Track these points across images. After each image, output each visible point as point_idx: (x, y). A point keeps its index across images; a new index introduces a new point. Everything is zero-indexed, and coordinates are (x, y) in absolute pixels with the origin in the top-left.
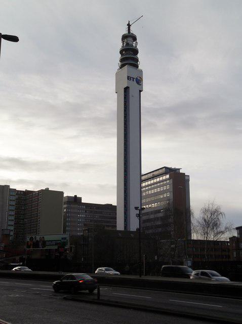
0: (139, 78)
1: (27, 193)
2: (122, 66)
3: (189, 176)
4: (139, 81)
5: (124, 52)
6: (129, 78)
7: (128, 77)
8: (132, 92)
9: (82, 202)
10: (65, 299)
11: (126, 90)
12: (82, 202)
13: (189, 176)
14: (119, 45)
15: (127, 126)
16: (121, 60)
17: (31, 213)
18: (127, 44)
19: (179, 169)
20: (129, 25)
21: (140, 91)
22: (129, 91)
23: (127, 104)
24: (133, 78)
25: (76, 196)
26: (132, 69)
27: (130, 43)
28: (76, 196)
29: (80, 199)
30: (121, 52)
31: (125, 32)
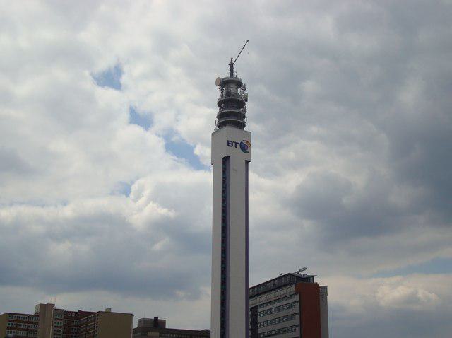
0: (245, 143)
1: (81, 314)
2: (221, 125)
3: (326, 288)
4: (245, 147)
5: (223, 105)
6: (229, 143)
7: (228, 141)
8: (235, 164)
9: (167, 327)
10: (175, 160)
11: (226, 160)
12: (167, 327)
13: (326, 288)
14: (217, 94)
15: (226, 245)
16: (220, 116)
17: (88, 323)
18: (228, 94)
19: (313, 277)
20: (232, 65)
21: (247, 162)
22: (229, 165)
23: (226, 240)
24: (236, 143)
25: (156, 318)
26: (235, 130)
27: (232, 90)
28: (156, 318)
29: (164, 322)
30: (219, 104)
31: (225, 74)
